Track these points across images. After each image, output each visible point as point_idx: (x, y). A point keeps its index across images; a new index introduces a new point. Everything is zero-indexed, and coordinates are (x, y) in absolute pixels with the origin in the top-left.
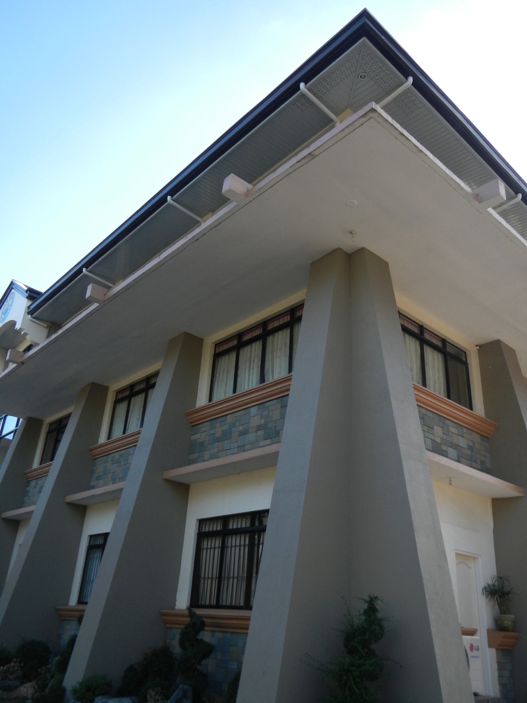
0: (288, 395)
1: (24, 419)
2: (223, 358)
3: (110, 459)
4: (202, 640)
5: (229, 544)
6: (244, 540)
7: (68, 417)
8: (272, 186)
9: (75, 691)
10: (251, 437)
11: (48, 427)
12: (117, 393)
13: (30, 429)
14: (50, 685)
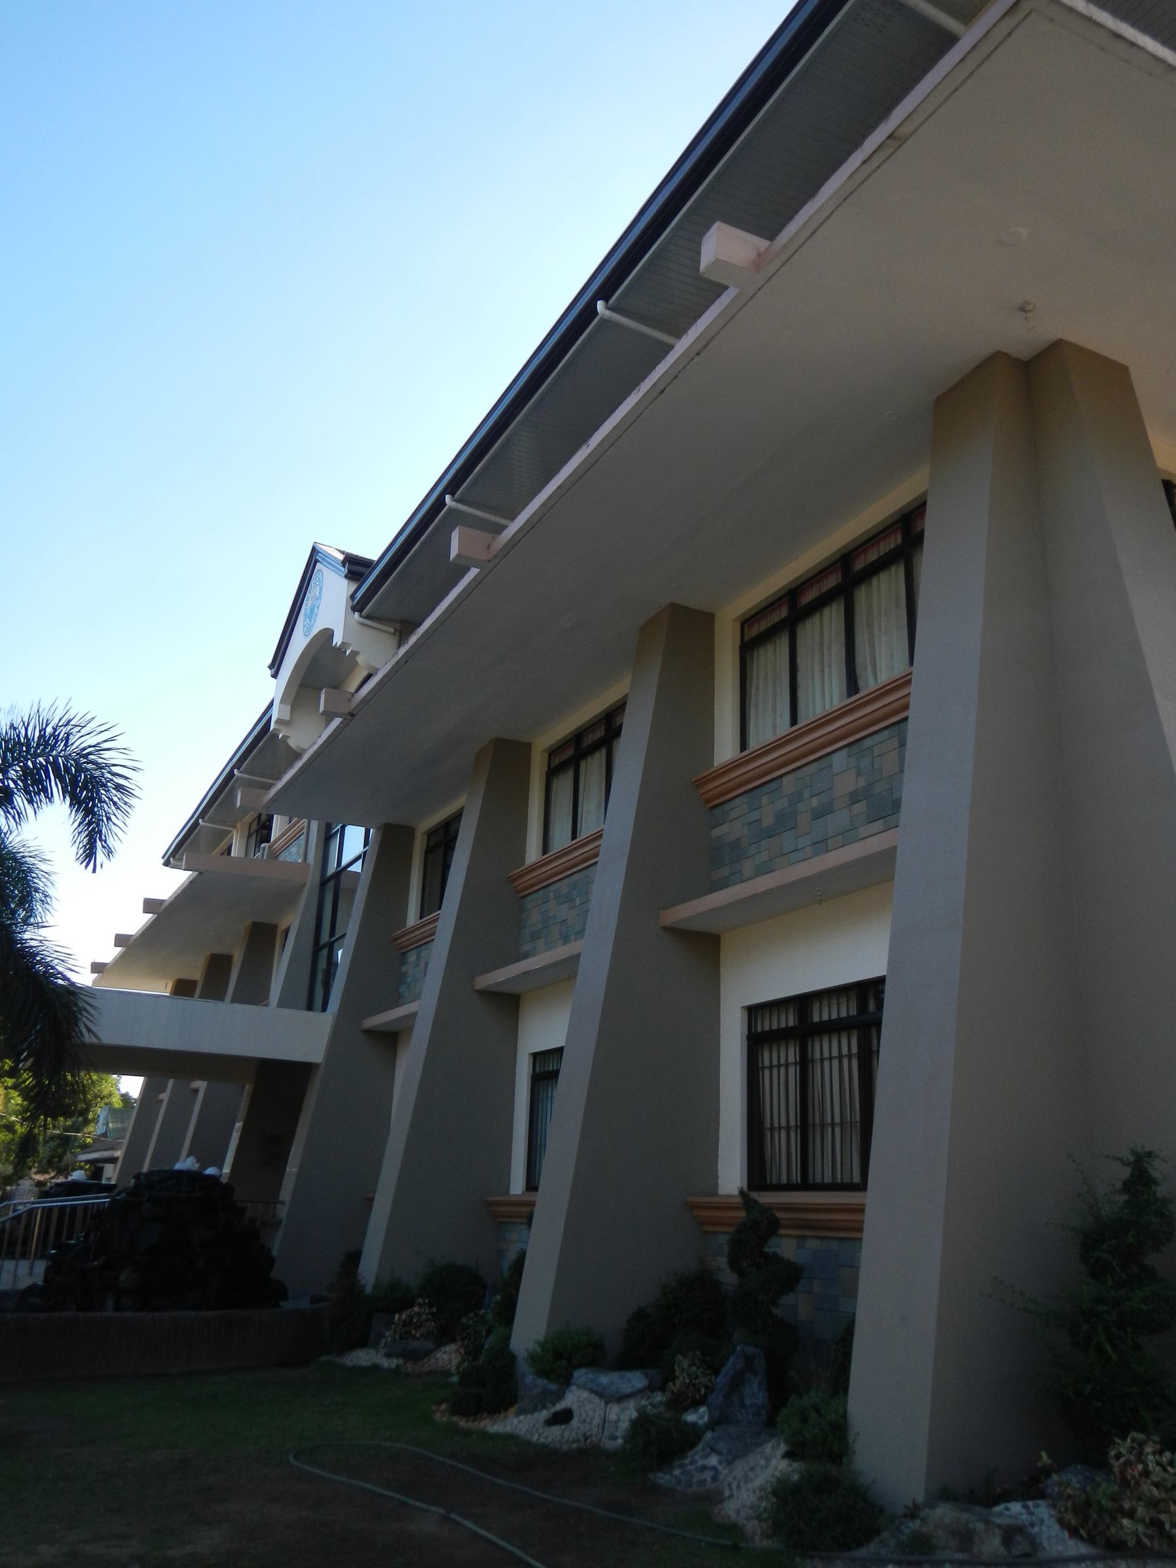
0: (906, 719)
1: (378, 829)
2: (762, 651)
3: (551, 895)
4: (775, 1255)
5: (817, 1055)
6: (849, 1044)
7: (457, 816)
8: (814, 233)
9: (533, 1358)
10: (838, 820)
11: (425, 840)
13: (390, 845)
14: (486, 1346)
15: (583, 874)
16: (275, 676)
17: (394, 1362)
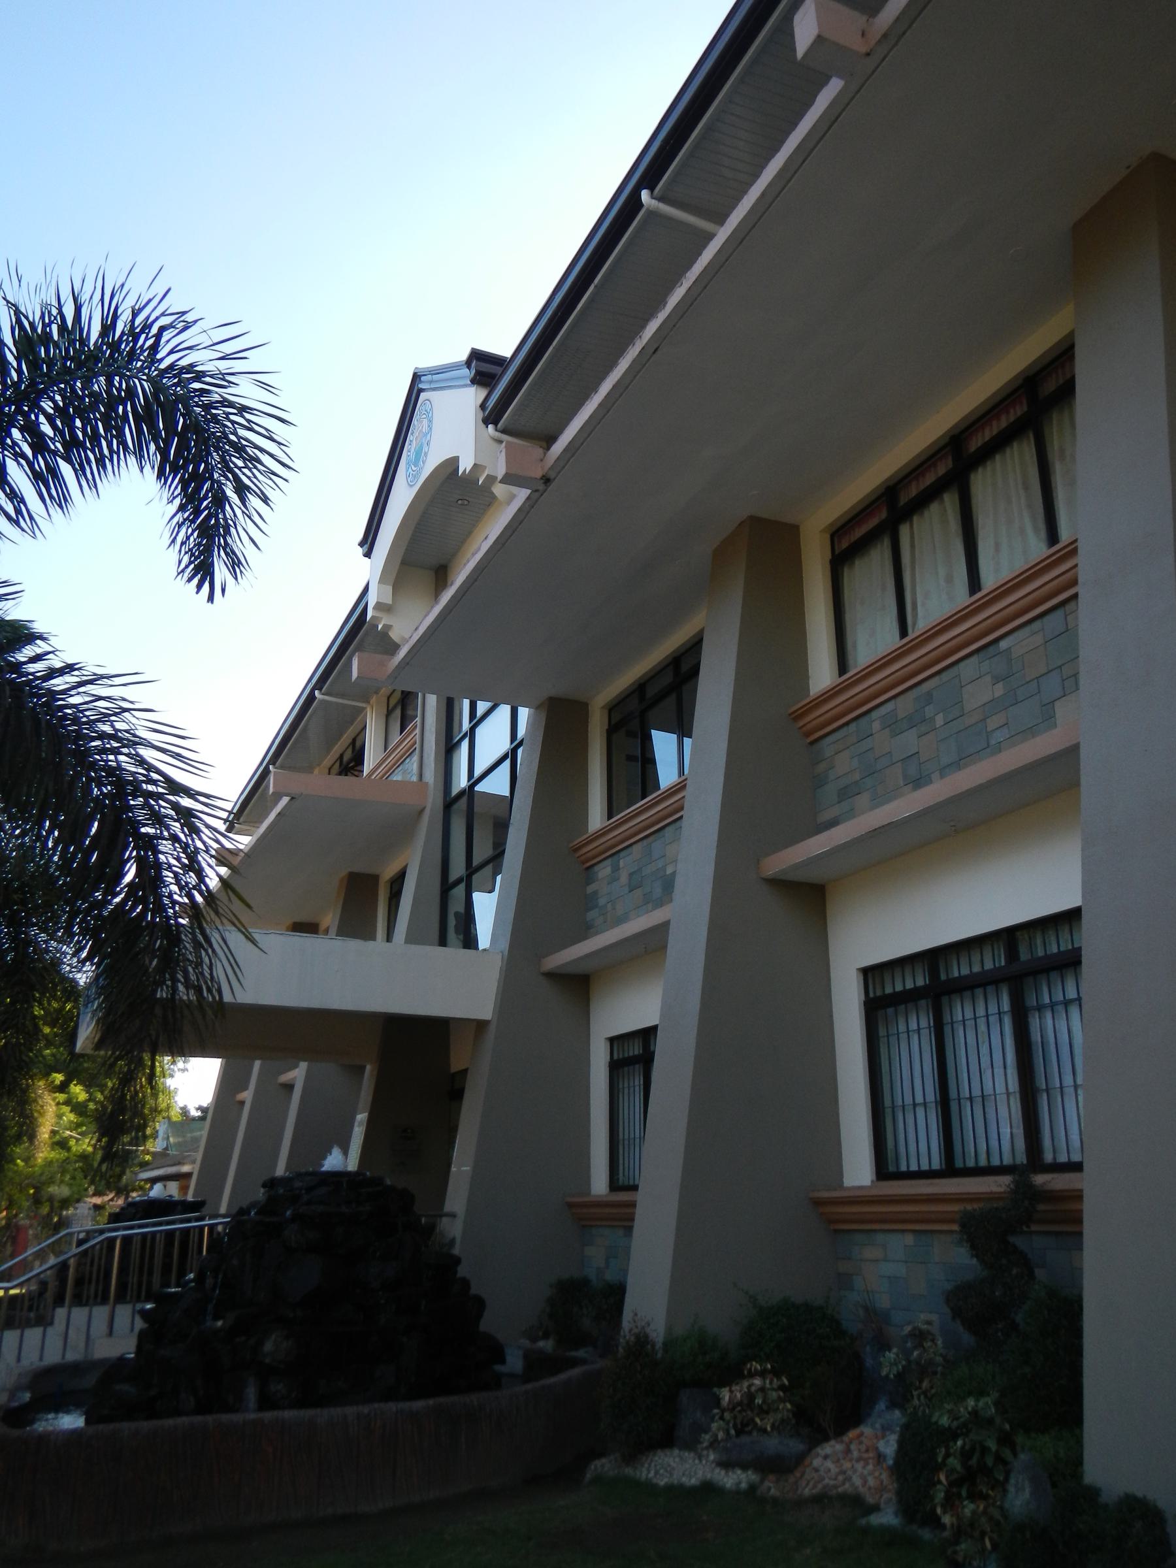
1: (537, 708)
3: (876, 726)
12: (832, 536)
15: (945, 676)
16: (368, 554)
17: (735, 1479)
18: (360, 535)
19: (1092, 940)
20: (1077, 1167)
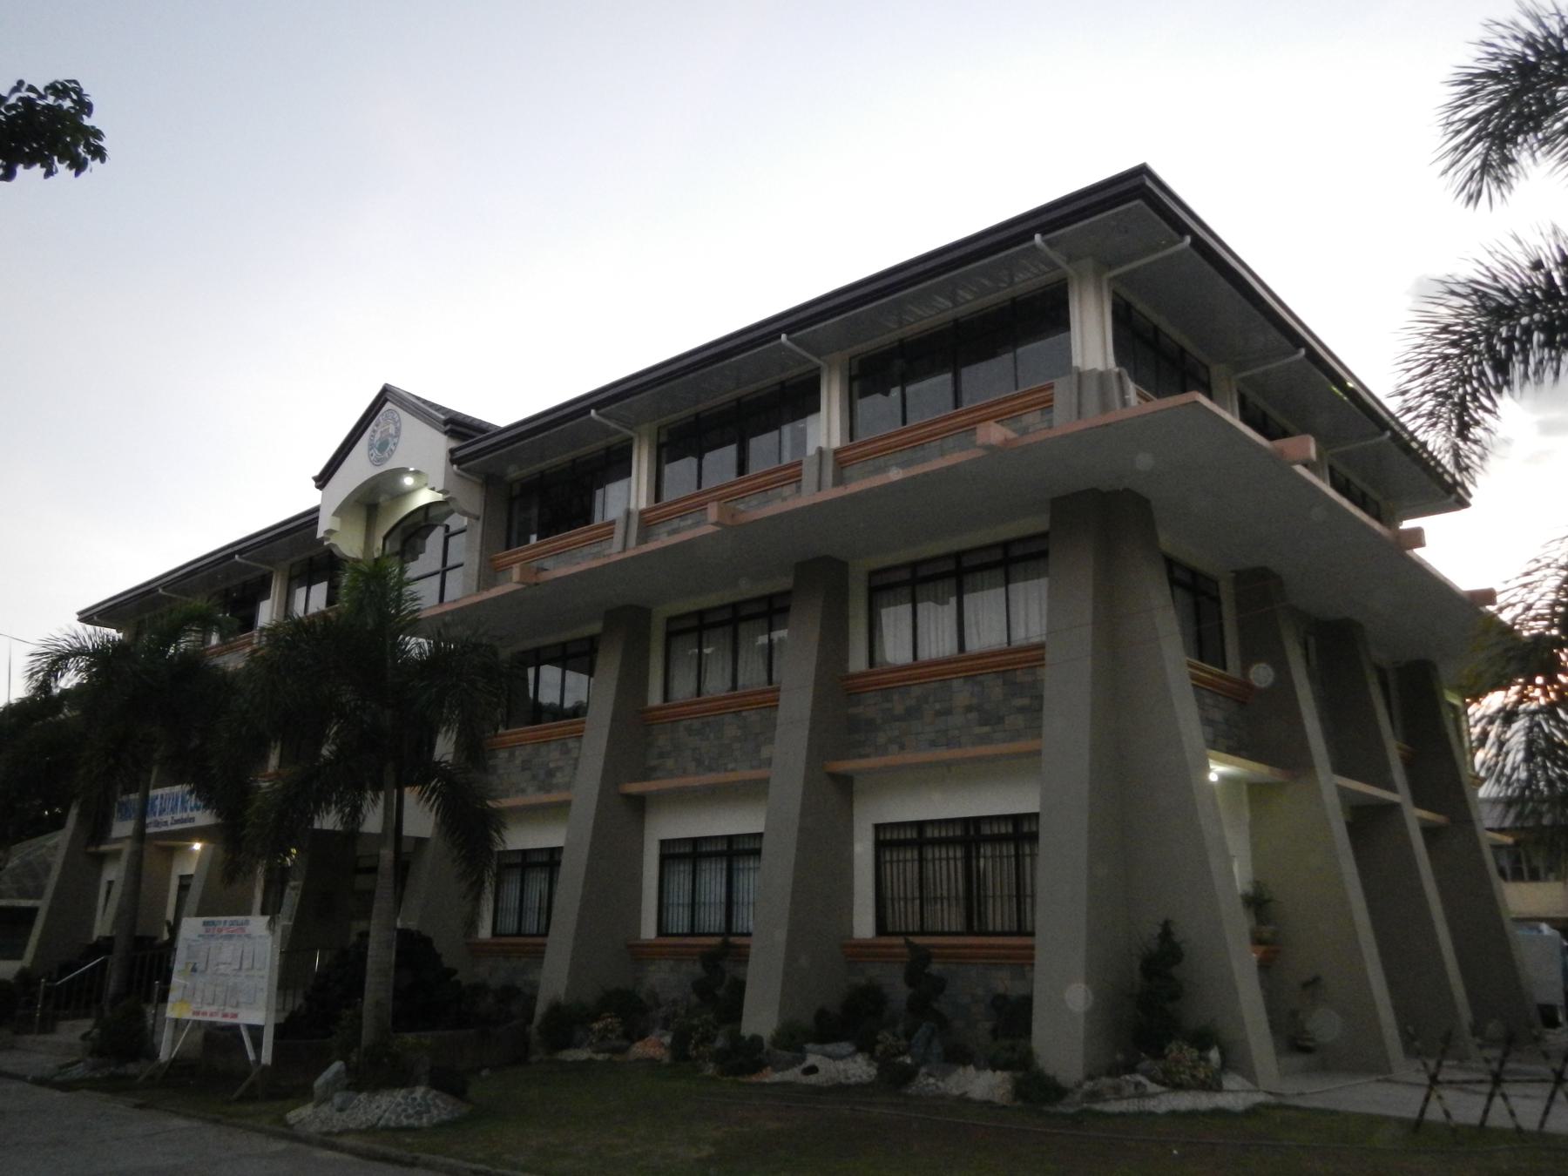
17: (600, 1057)
18: (317, 472)
19: (767, 846)
20: (749, 934)
